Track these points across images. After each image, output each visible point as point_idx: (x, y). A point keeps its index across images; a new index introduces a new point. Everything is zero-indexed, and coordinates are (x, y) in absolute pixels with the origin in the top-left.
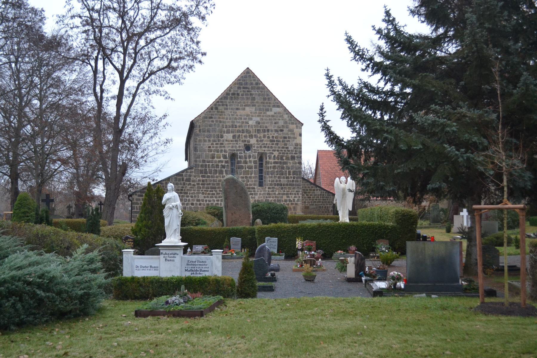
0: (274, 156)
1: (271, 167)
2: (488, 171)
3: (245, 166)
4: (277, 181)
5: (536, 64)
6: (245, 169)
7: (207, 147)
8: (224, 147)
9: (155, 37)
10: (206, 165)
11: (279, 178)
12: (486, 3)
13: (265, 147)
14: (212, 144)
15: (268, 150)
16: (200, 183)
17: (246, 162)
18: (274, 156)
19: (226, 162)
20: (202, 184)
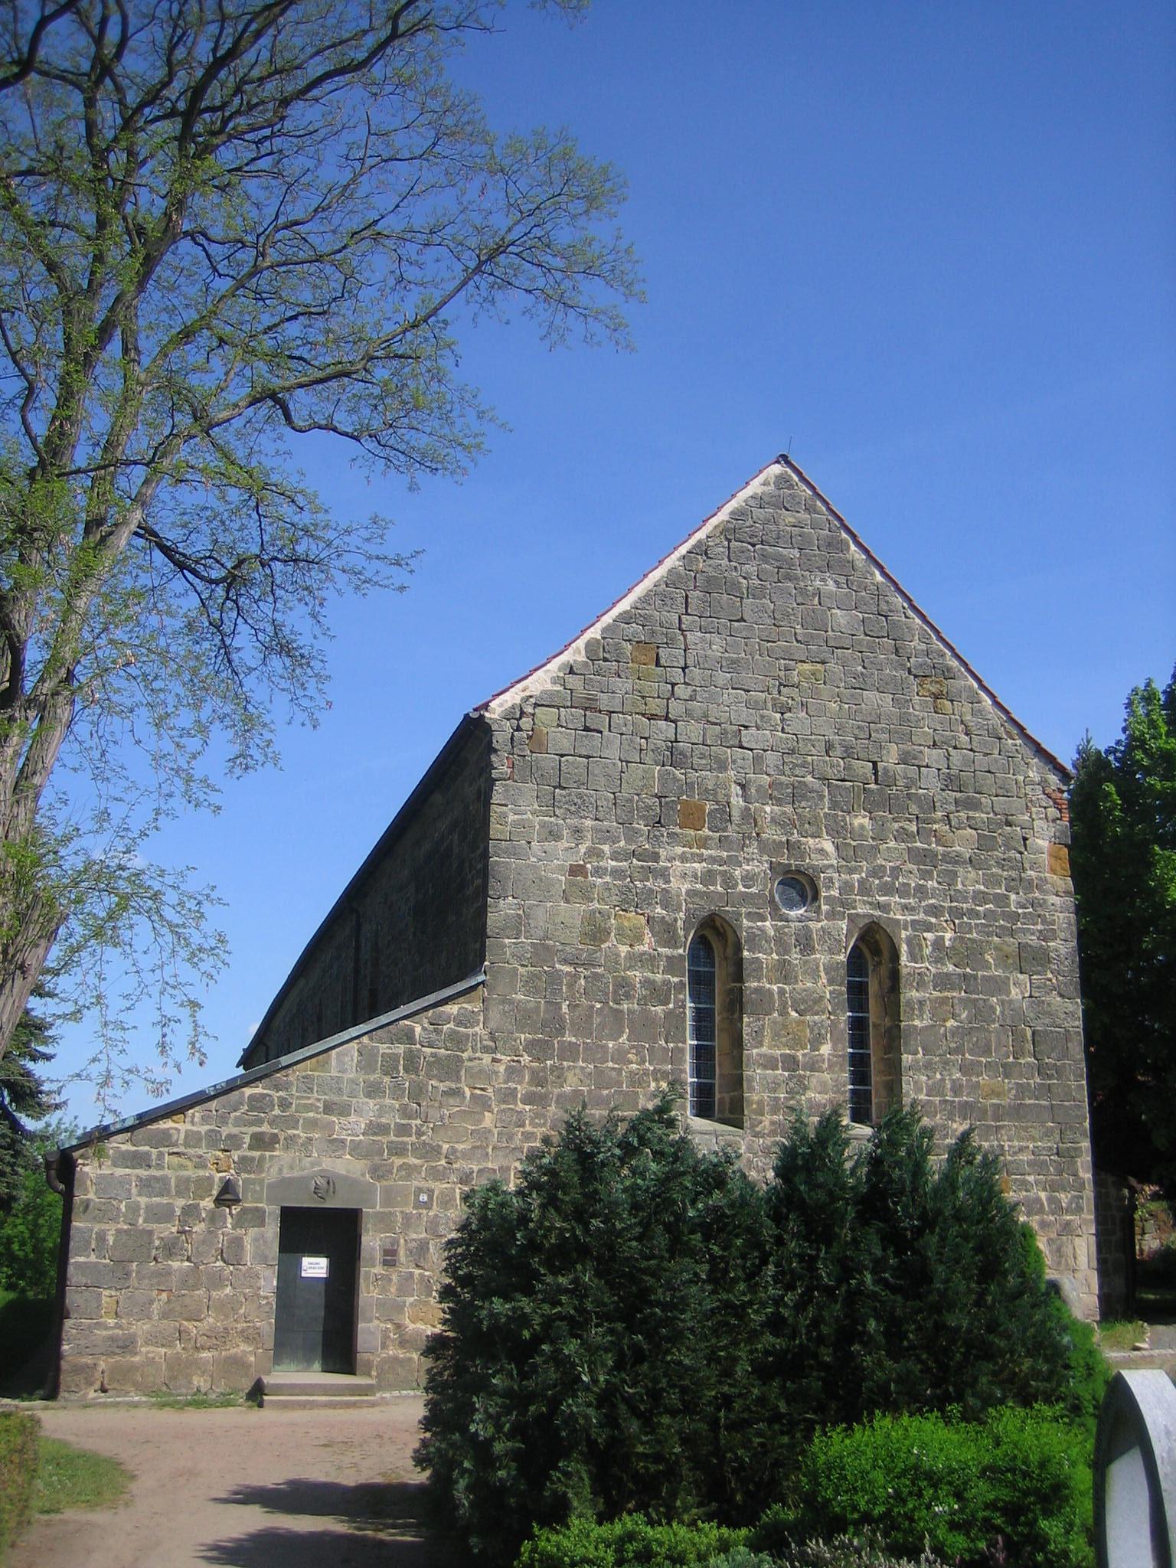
0: (938, 943)
1: (921, 1003)
2: (990, 1472)
3: (782, 992)
4: (957, 1090)
5: (1167, 1255)
6: (784, 1013)
7: (560, 869)
8: (664, 874)
9: (212, 45)
10: (555, 978)
11: (966, 1069)
12: (772, 1542)
13: (888, 889)
14: (594, 853)
15: (906, 908)
16: (521, 1089)
17: (784, 971)
18: (938, 943)
19: (672, 964)
20: (529, 1099)
